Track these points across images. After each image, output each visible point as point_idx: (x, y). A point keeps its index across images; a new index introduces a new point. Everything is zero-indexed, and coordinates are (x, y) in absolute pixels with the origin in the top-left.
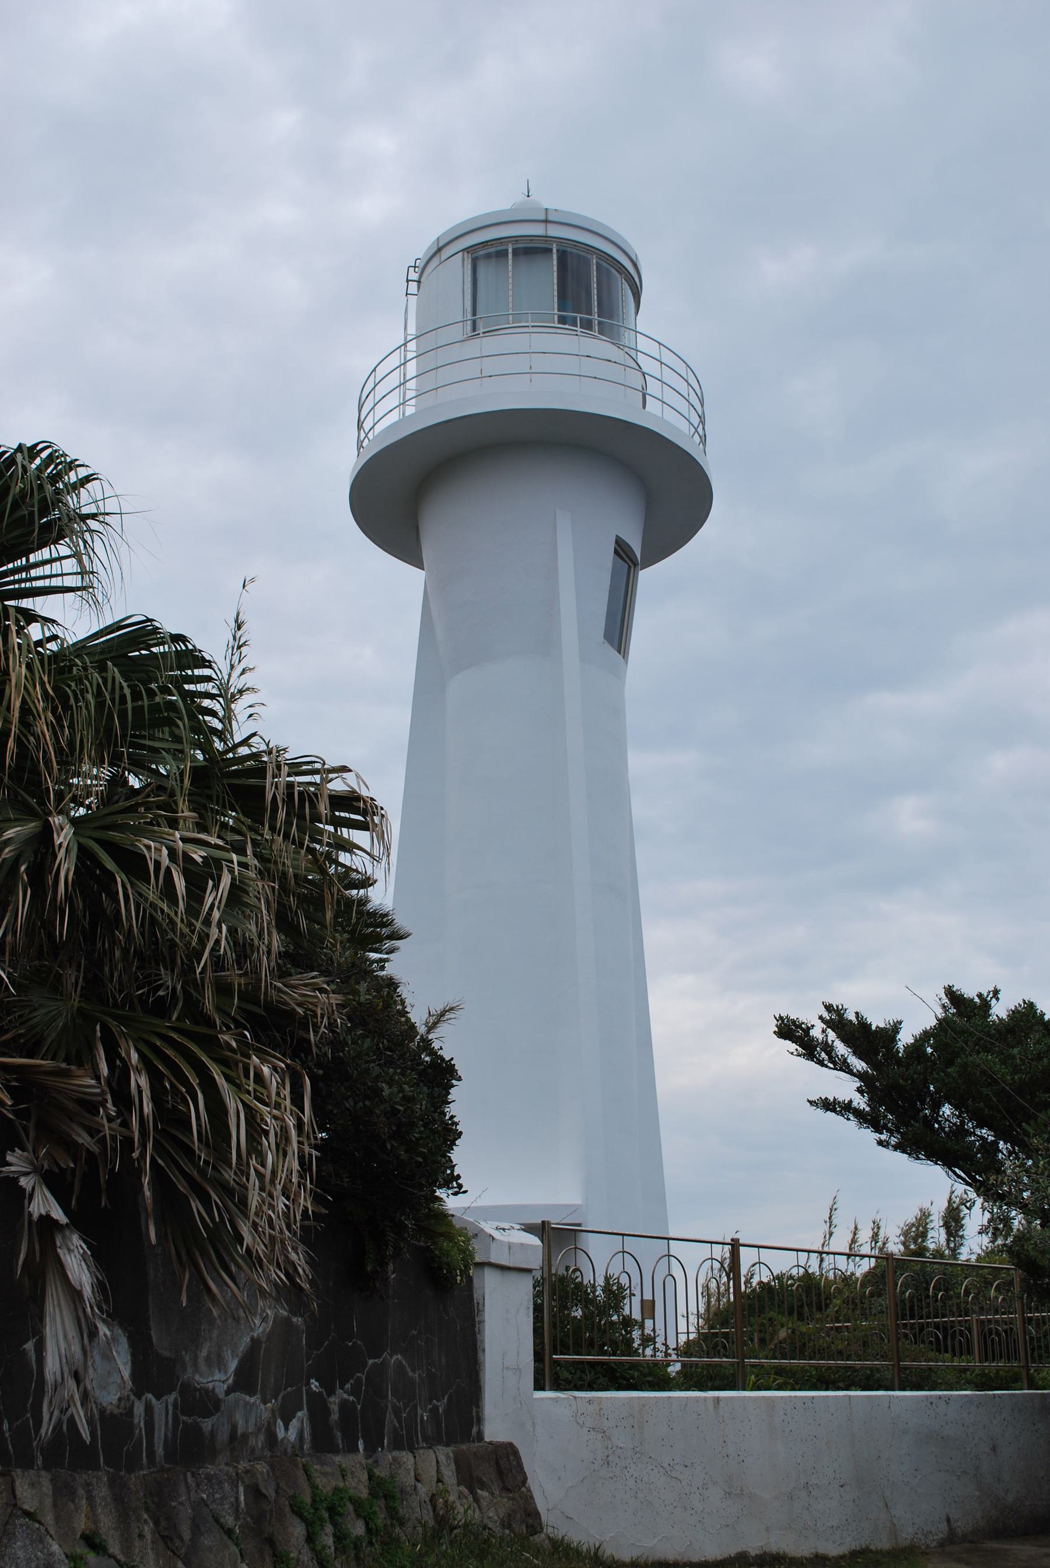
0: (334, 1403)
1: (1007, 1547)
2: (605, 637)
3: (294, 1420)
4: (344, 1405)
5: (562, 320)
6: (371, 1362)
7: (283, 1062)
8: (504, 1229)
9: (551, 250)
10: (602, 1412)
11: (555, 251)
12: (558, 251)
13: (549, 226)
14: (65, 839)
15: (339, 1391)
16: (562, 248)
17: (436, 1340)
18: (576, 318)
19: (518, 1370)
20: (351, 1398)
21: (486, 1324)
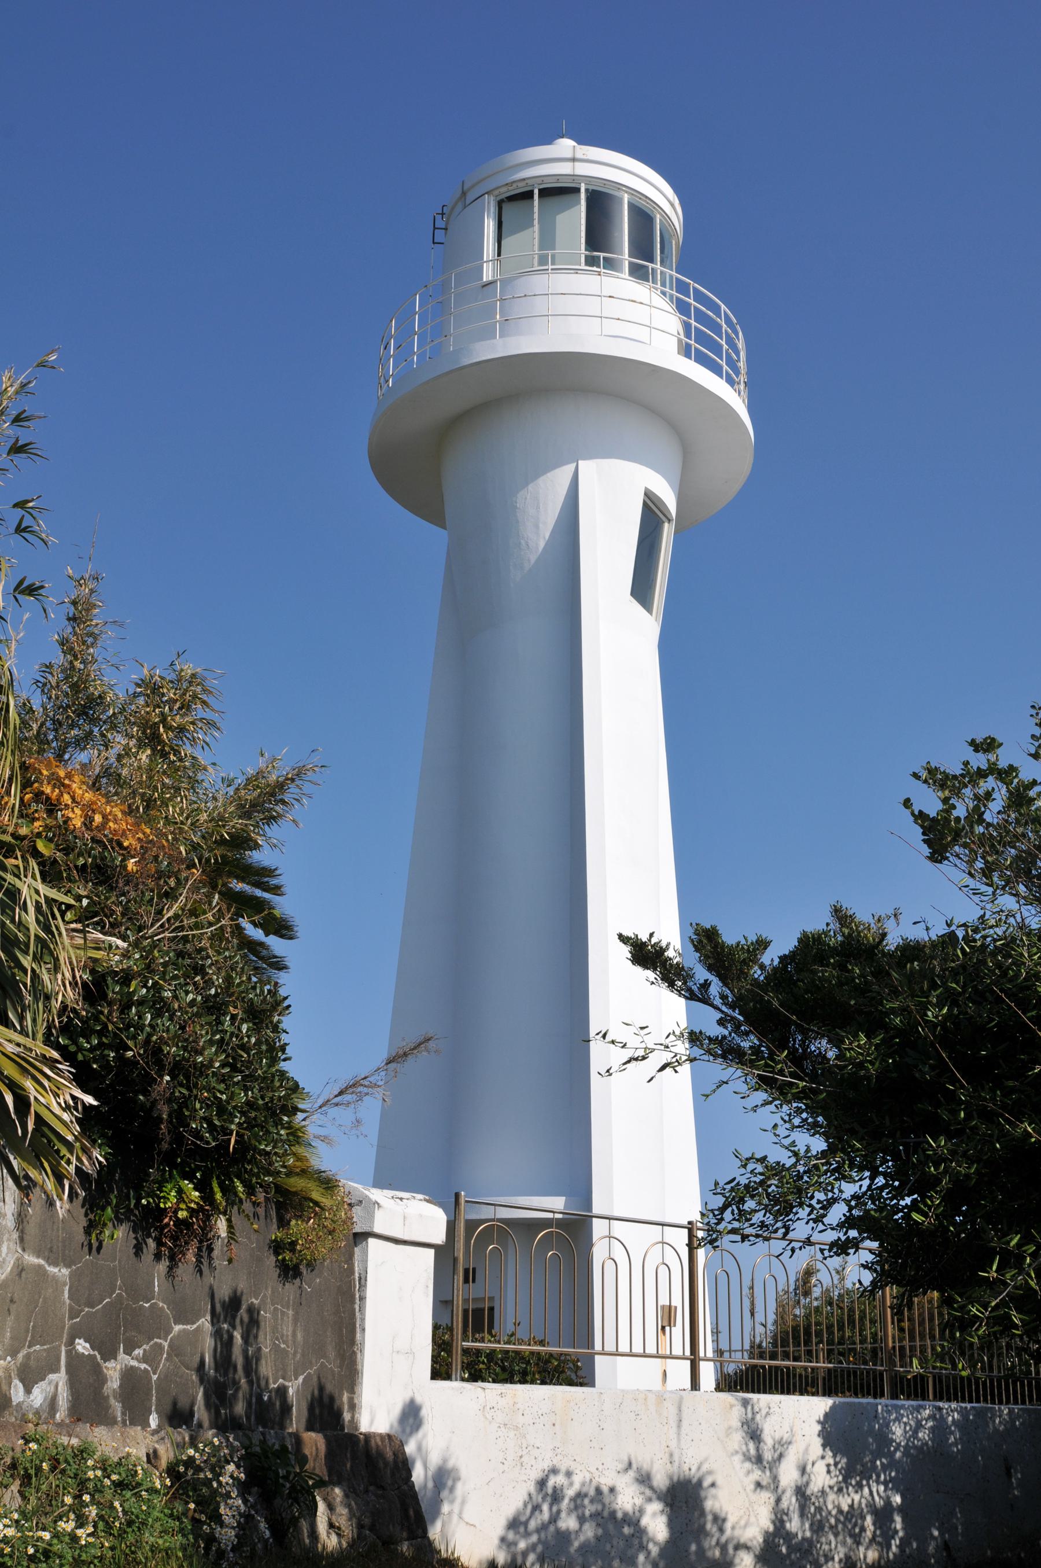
0: (113, 1371)
1: (274, 1220)
2: (632, 594)
3: (43, 1384)
4: (129, 1375)
5: (591, 261)
6: (177, 1328)
7: (894, 1342)
8: (401, 1199)
9: (577, 190)
10: (517, 1406)
11: (583, 190)
12: (587, 190)
13: (577, 164)
14: (15, 799)
15: (122, 1356)
16: (591, 188)
17: (291, 1312)
18: (599, 257)
19: (410, 1353)
20: (143, 1366)
21: (368, 1300)
